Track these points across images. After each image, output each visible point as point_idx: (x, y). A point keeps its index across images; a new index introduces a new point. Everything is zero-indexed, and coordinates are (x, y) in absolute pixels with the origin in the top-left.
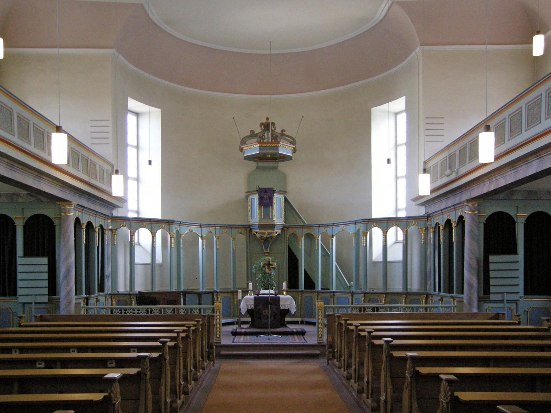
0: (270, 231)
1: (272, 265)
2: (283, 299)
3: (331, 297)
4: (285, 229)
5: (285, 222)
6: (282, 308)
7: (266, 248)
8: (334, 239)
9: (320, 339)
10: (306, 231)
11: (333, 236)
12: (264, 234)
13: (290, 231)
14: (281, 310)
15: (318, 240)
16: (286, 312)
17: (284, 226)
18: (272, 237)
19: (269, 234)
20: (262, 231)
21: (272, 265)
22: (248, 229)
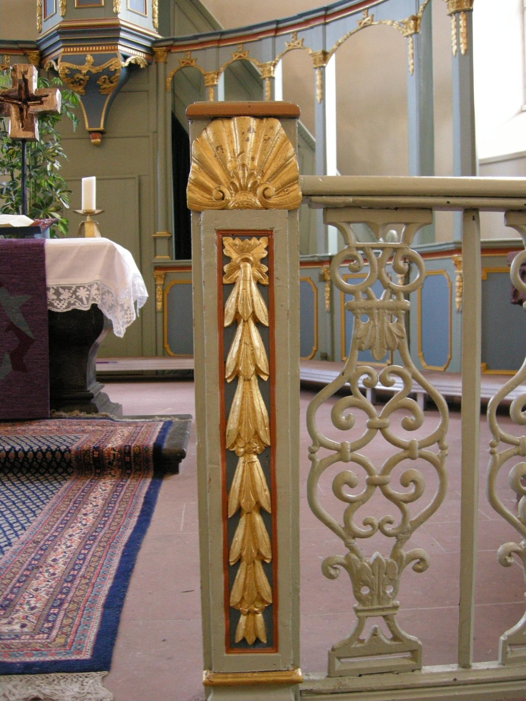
0: (102, 49)
1: (38, 99)
2: (63, 252)
3: (322, 278)
4: (160, 51)
5: (160, 31)
6: (61, 307)
7: (94, 119)
8: (331, 67)
9: (251, 664)
10: (229, 54)
11: (325, 55)
12: (82, 61)
13: (177, 59)
14: (53, 315)
15: (272, 79)
16: (90, 323)
17: (156, 42)
18: (110, 74)
19: (98, 60)
20: (75, 50)
21: (38, 99)
22: (34, 54)
